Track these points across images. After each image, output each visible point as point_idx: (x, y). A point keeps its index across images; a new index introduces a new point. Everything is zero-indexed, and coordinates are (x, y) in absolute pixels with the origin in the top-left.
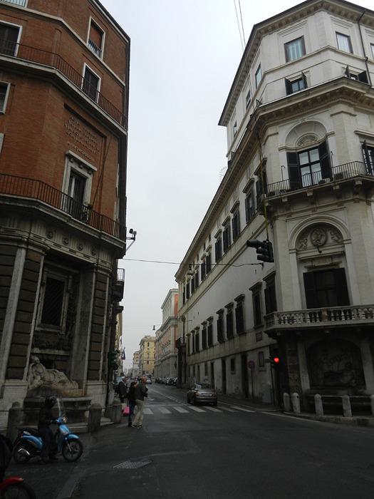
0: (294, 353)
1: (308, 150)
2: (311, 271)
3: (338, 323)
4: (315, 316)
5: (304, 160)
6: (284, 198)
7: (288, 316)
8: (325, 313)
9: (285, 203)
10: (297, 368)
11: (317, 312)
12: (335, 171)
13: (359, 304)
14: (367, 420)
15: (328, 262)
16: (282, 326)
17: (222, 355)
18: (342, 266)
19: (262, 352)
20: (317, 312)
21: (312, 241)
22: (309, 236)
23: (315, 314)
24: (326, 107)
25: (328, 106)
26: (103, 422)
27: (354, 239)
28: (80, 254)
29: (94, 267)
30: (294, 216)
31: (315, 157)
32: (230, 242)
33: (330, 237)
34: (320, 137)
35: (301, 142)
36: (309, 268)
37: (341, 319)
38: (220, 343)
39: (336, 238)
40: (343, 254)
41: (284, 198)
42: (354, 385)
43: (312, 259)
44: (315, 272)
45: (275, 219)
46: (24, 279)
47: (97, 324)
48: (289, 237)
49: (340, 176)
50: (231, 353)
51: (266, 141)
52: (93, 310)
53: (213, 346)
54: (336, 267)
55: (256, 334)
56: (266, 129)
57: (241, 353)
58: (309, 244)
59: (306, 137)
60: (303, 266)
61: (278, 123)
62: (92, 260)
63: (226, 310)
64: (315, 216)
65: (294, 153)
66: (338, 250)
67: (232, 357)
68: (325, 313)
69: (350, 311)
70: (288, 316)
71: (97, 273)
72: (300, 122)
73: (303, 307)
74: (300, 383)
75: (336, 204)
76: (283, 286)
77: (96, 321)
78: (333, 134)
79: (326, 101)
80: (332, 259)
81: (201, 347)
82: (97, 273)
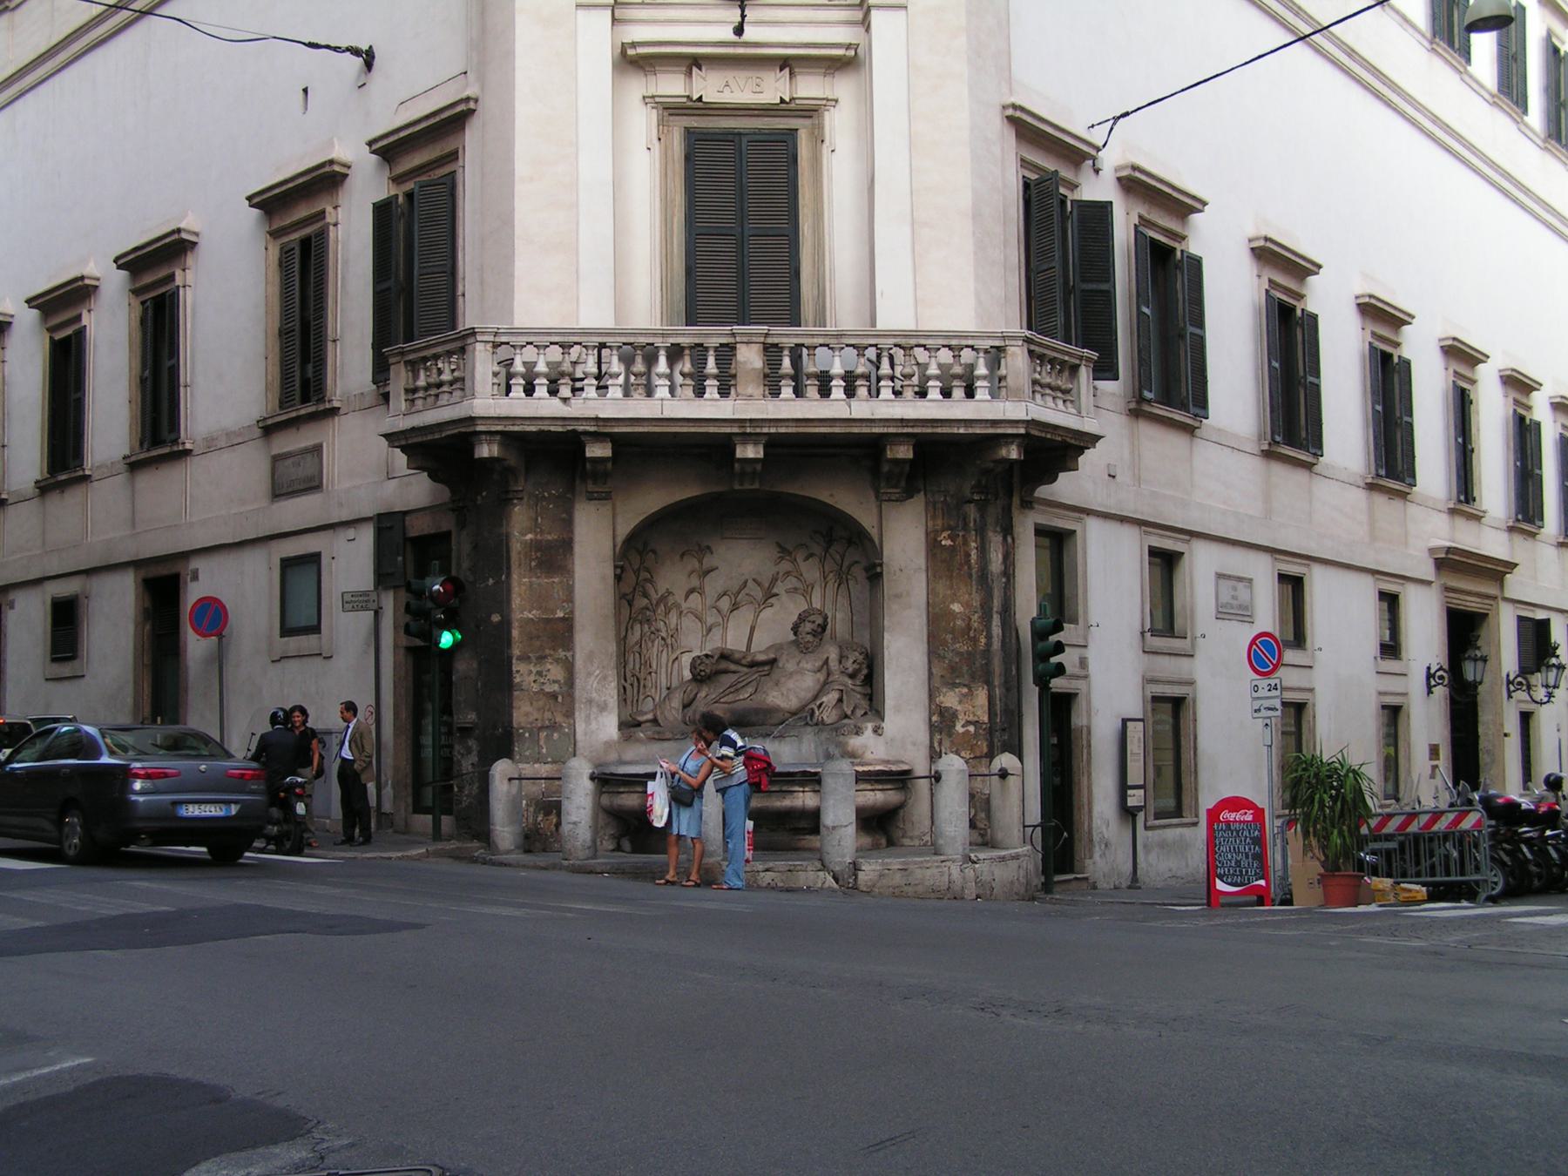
7: (945, 356)
8: (750, 357)
10: (560, 633)
11: (714, 342)
13: (907, 324)
16: (517, 405)
19: (315, 558)
37: (650, 392)
40: (845, 63)
42: (829, 716)
43: (693, 63)
55: (276, 459)
57: (136, 564)
63: (114, 284)
68: (750, 357)
70: (555, 353)
74: (570, 714)
80: (635, 47)
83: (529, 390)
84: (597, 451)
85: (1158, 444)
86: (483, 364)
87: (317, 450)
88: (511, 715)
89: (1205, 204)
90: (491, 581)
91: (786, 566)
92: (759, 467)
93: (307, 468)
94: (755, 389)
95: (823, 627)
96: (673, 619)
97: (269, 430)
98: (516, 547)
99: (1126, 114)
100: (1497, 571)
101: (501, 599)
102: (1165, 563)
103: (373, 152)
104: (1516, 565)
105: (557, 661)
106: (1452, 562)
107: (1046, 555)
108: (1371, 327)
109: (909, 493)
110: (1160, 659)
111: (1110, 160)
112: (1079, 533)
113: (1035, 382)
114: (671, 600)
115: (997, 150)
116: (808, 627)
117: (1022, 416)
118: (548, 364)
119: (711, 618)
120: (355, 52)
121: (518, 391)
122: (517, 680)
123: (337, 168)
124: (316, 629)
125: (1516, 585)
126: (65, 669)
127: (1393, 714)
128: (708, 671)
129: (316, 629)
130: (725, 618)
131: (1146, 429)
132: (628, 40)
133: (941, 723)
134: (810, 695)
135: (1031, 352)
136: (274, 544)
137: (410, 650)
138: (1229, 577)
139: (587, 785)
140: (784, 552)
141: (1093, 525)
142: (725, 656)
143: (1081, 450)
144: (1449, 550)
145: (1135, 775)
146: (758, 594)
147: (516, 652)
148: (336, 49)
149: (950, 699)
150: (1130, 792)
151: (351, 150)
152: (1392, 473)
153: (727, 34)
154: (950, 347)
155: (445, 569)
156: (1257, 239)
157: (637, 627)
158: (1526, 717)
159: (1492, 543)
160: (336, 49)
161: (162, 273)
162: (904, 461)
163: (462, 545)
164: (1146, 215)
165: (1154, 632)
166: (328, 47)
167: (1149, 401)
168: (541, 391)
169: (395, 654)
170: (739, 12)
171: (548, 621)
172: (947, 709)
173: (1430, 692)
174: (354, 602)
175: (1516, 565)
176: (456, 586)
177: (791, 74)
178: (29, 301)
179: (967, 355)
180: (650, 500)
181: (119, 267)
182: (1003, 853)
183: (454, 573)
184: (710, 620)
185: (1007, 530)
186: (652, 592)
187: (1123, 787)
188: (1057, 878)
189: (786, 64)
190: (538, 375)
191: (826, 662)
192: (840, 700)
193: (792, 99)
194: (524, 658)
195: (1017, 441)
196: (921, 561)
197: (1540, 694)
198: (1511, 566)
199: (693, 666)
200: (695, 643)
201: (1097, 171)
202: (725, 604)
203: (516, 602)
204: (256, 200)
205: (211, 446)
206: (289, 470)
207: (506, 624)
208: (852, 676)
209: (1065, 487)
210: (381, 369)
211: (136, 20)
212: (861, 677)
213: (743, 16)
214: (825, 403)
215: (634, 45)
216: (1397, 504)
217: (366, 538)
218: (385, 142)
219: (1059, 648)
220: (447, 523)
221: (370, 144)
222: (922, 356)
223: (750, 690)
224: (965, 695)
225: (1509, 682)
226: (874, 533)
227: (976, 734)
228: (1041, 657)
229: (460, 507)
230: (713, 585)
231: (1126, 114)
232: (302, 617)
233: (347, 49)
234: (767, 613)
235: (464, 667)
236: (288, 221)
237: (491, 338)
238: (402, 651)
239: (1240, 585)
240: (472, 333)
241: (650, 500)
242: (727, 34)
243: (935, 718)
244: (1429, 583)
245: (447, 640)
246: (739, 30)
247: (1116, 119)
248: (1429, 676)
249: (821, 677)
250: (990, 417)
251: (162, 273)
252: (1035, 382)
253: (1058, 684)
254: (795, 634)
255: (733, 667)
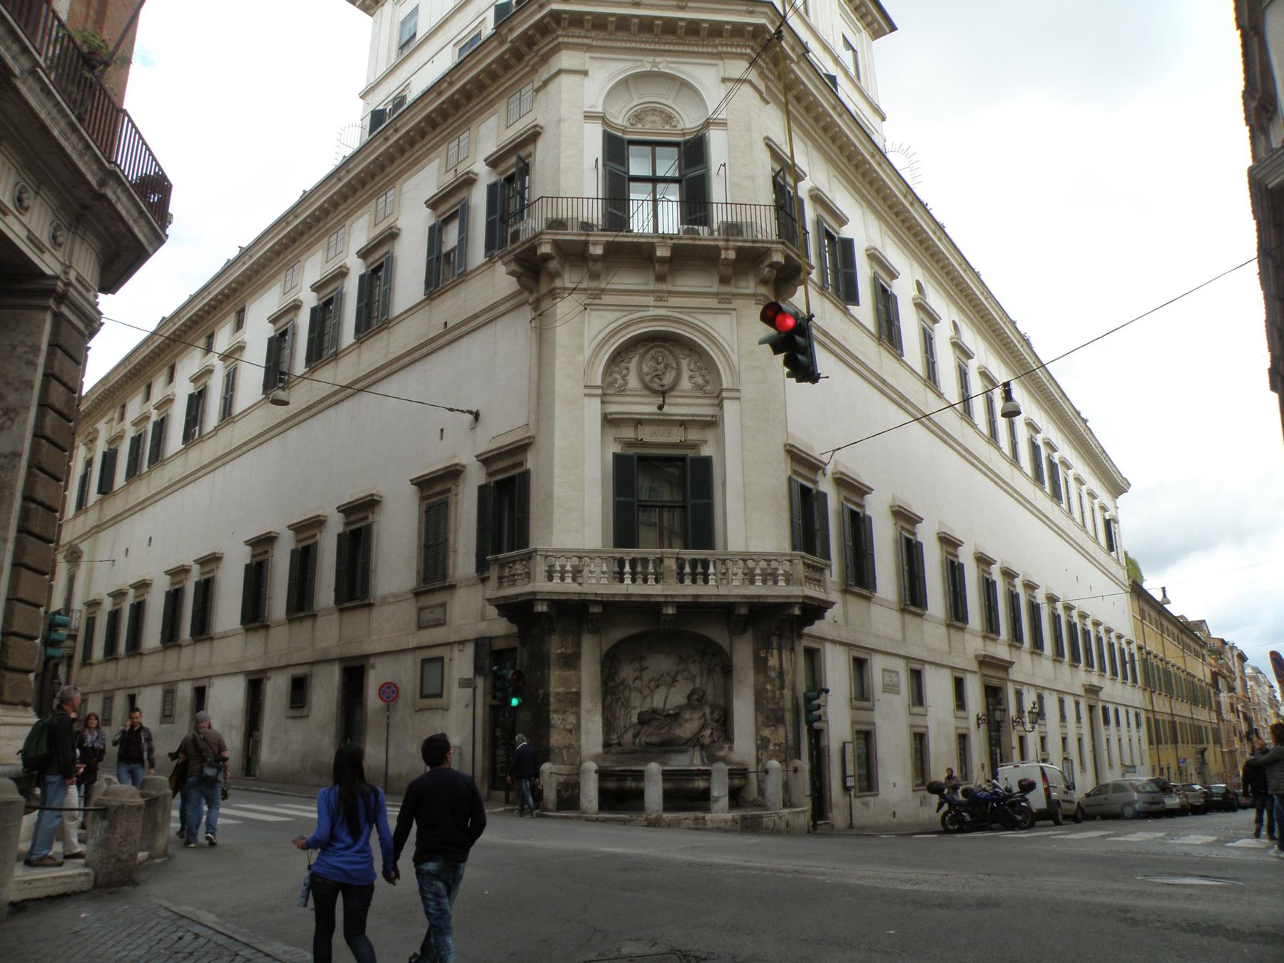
0: (571, 661)
1: (654, 144)
2: (631, 451)
3: (699, 590)
4: (681, 567)
5: (638, 165)
6: (596, 243)
7: (763, 564)
8: (671, 564)
9: (596, 259)
10: (574, 700)
11: (651, 557)
12: (720, 215)
14: (761, 817)
15: (676, 436)
16: (556, 586)
17: (251, 666)
18: (706, 451)
20: (651, 557)
21: (641, 377)
22: (635, 361)
23: (621, 563)
24: (712, 55)
25: (719, 56)
26: (397, 806)
27: (748, 392)
28: (17, 227)
29: (50, 292)
30: (606, 299)
31: (668, 165)
32: (336, 339)
33: (685, 375)
34: (689, 121)
35: (638, 117)
36: (628, 444)
38: (247, 630)
39: (700, 380)
40: (713, 424)
41: (596, 243)
42: (707, 741)
43: (638, 422)
44: (642, 459)
45: (553, 294)
46: (157, 231)
47: (42, 504)
48: (588, 352)
49: (733, 229)
50: (295, 660)
51: (546, 83)
52: (35, 450)
53: (91, 664)
54: (690, 453)
55: (420, 610)
56: (557, 49)
57: (341, 660)
58: (633, 382)
59: (654, 110)
60: (612, 433)
61: (589, 48)
62: (48, 264)
64: (662, 312)
65: (621, 140)
66: (702, 409)
67: (299, 671)
69: (705, 564)
71: (58, 317)
72: (647, 68)
73: (604, 543)
74: (578, 740)
75: (716, 295)
76: (557, 481)
77: (40, 494)
78: (723, 124)
79: (717, 41)
81: (98, 651)
82: (58, 317)
83: (562, 579)
84: (595, 609)
85: (855, 605)
86: (540, 567)
87: (443, 605)
88: (549, 741)
89: (872, 490)
90: (539, 673)
91: (682, 666)
92: (673, 618)
93: (437, 614)
94: (674, 580)
95: (703, 697)
96: (627, 693)
97: (417, 594)
98: (553, 656)
99: (840, 449)
100: (1005, 666)
101: (545, 682)
102: (860, 665)
103: (479, 461)
104: (1014, 663)
105: (573, 713)
106: (986, 662)
107: (915, 682)
108: (945, 548)
109: (744, 631)
110: (860, 712)
111: (830, 469)
112: (822, 651)
113: (806, 577)
114: (626, 683)
115: (783, 465)
116: (695, 697)
117: (800, 593)
118: (572, 566)
119: (646, 692)
120: (471, 412)
121: (557, 580)
122: (552, 722)
123: (458, 468)
124: (440, 695)
125: (1015, 674)
126: (298, 713)
127: (963, 739)
128: (646, 719)
129: (440, 695)
130: (652, 691)
131: (850, 598)
132: (608, 411)
133: (762, 744)
134: (696, 731)
135: (804, 563)
136: (418, 652)
137: (492, 707)
138: (888, 671)
139: (595, 777)
140: (682, 660)
141: (828, 646)
142: (654, 711)
143: (825, 610)
144: (985, 656)
145: (850, 769)
146: (669, 679)
147: (552, 708)
148: (462, 411)
149: (766, 733)
150: (848, 779)
151: (467, 458)
152: (958, 619)
153: (654, 409)
154: (765, 560)
155: (513, 667)
156: (894, 506)
157: (609, 697)
158: (1021, 739)
159: (1001, 650)
160: (462, 411)
161: (362, 515)
162: (743, 615)
163: (523, 656)
164: (848, 496)
165: (914, 704)
166: (458, 410)
167: (851, 585)
168: (569, 580)
169: (484, 708)
170: (662, 399)
171: (567, 693)
172: (766, 737)
173: (979, 726)
174: (465, 683)
175: (1014, 663)
176: (519, 675)
177: (685, 429)
178: (290, 527)
179: (774, 564)
180: (617, 634)
181: (339, 512)
182: (798, 810)
183: (518, 668)
184: (646, 693)
185: (792, 650)
186: (616, 679)
187: (844, 777)
188: (819, 822)
189: (683, 424)
190: (567, 572)
191: (704, 714)
192: (712, 733)
193: (686, 440)
194: (556, 712)
195: (798, 605)
196: (751, 664)
197: (1028, 727)
198: (1012, 663)
199: (640, 715)
200: (639, 704)
201: (825, 475)
202: (653, 685)
203: (553, 683)
204: (415, 481)
205: (384, 601)
206: (427, 615)
207: (547, 695)
208: (717, 721)
209: (818, 628)
210: (482, 565)
211: (356, 393)
212: (721, 722)
213: (664, 402)
214: (706, 587)
215: (611, 414)
216: (960, 634)
217: (470, 650)
218: (485, 456)
219: (819, 707)
220: (515, 643)
221: (477, 456)
222: (751, 564)
223: (667, 728)
224: (773, 731)
225: (1013, 721)
226: (728, 650)
227: (779, 750)
228: (809, 711)
229: (523, 635)
230: (647, 676)
231: (840, 449)
232: (432, 687)
233: (467, 412)
234: (673, 690)
235: (524, 716)
236: (431, 492)
237: (544, 553)
238: (487, 708)
239: (893, 675)
240: (535, 550)
241: (617, 634)
242: (654, 409)
243: (759, 742)
244: (975, 672)
245: (515, 702)
246: (661, 407)
247: (834, 451)
248: (978, 719)
249: (702, 722)
250: (786, 594)
251: (362, 515)
252: (806, 577)
253: (816, 725)
254: (689, 700)
255: (659, 717)
